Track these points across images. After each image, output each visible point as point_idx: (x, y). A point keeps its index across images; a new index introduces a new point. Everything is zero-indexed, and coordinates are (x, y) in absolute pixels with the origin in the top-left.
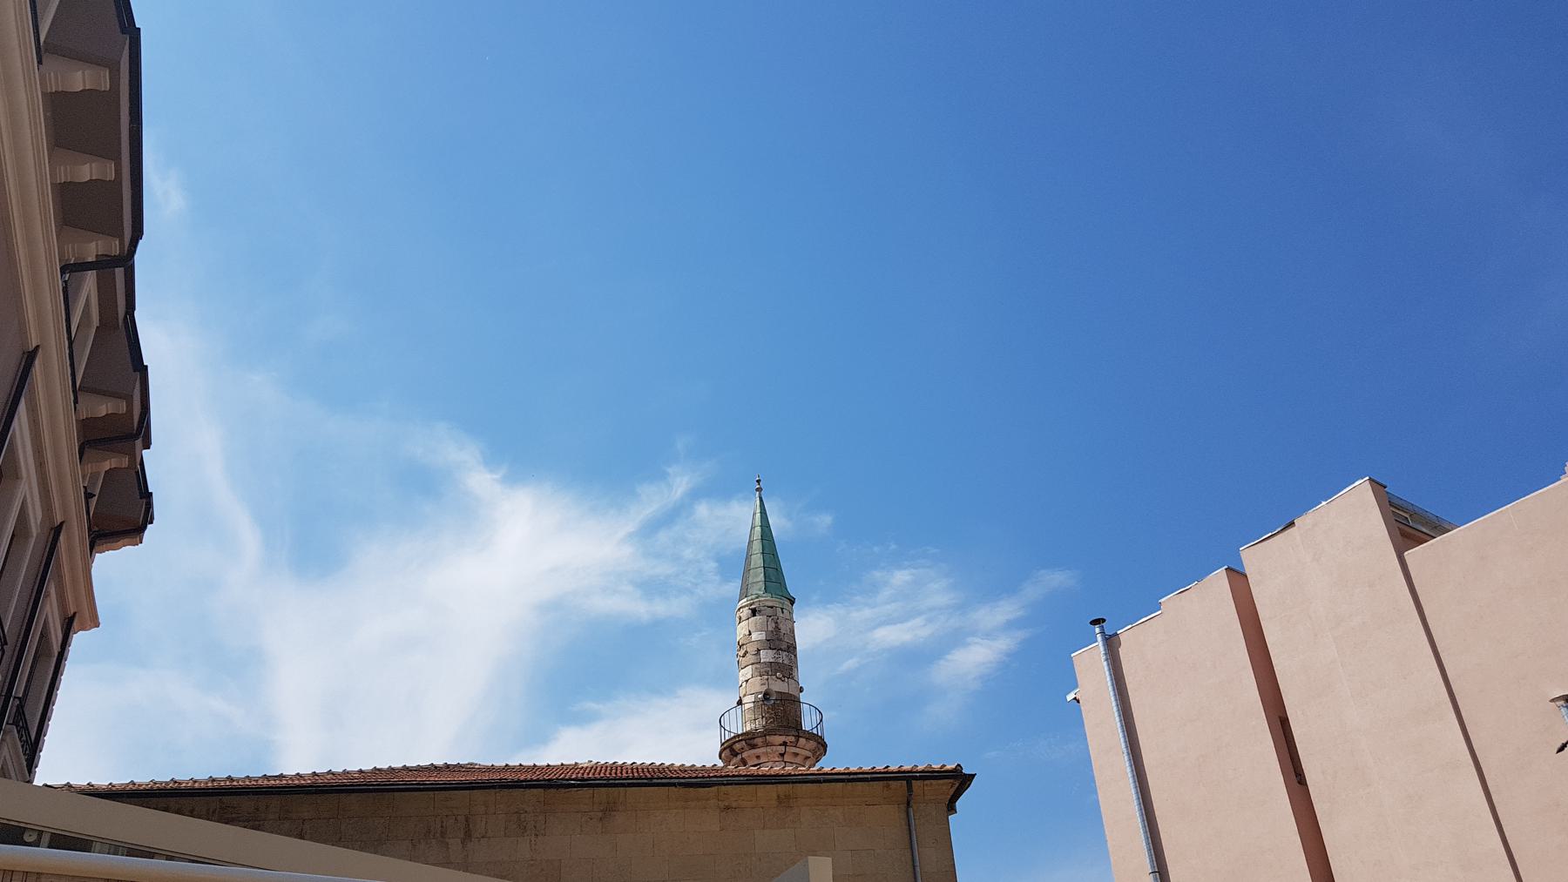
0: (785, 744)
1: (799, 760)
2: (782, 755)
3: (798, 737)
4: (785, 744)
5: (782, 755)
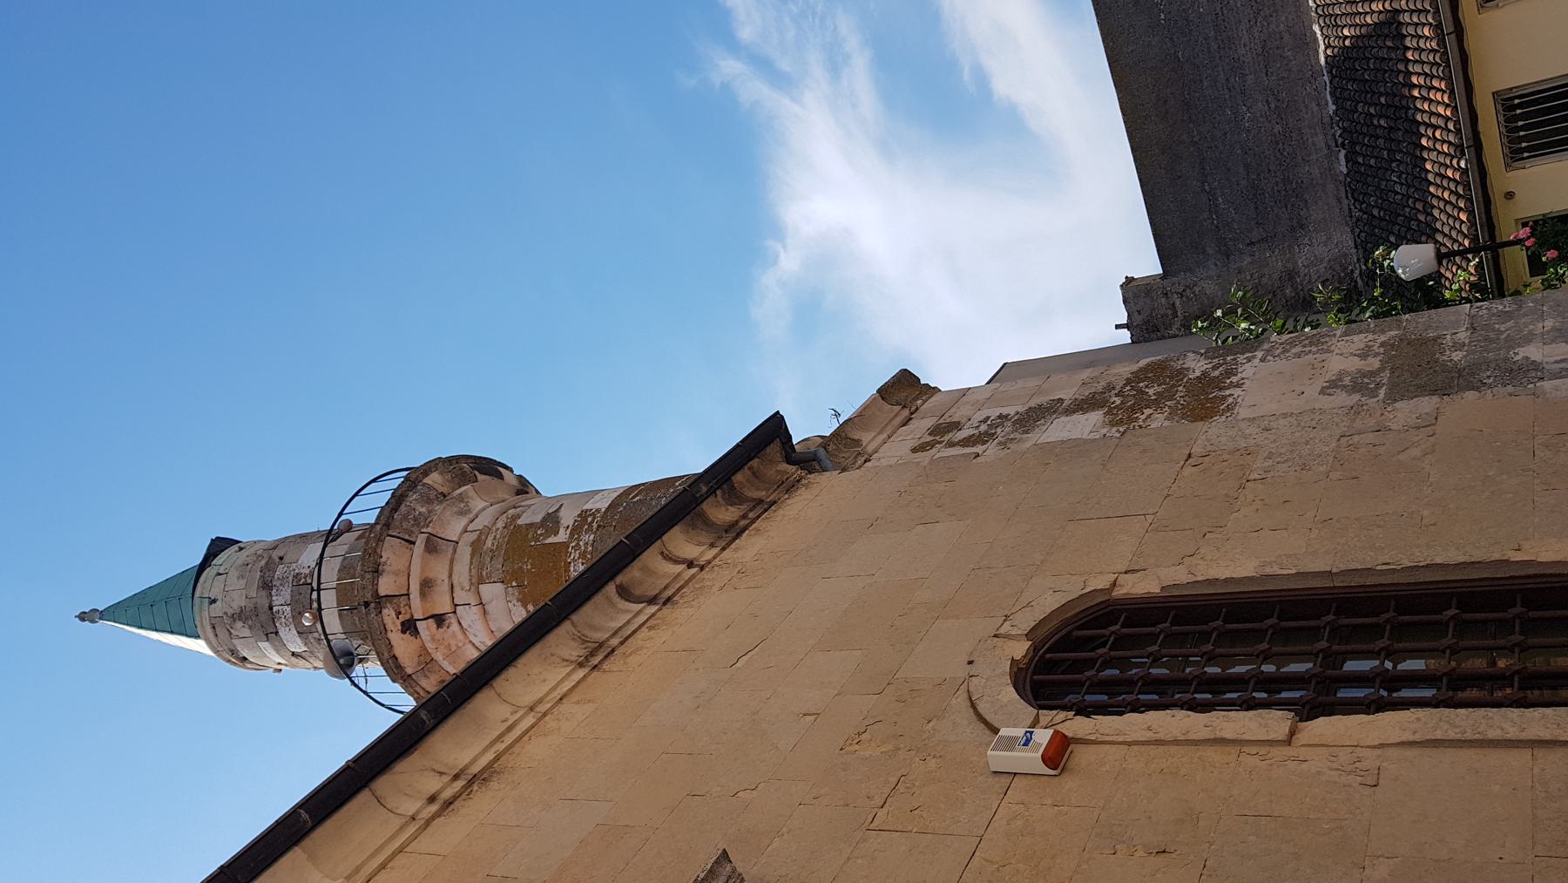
0: (409, 627)
1: (439, 570)
2: (440, 620)
3: (380, 601)
4: (409, 627)
5: (440, 620)
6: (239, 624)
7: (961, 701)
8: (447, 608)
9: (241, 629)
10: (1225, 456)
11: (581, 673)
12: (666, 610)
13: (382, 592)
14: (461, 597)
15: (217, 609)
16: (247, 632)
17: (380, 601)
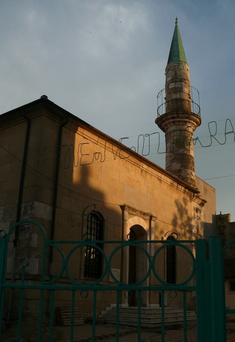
0: (173, 118)
5: (174, 122)
6: (174, 73)
7: (167, 231)
8: (176, 124)
9: (173, 73)
10: (141, 168)
11: (170, 184)
12: (176, 189)
13: (179, 115)
14: (178, 127)
15: (176, 68)
16: (173, 75)
17: (178, 114)
